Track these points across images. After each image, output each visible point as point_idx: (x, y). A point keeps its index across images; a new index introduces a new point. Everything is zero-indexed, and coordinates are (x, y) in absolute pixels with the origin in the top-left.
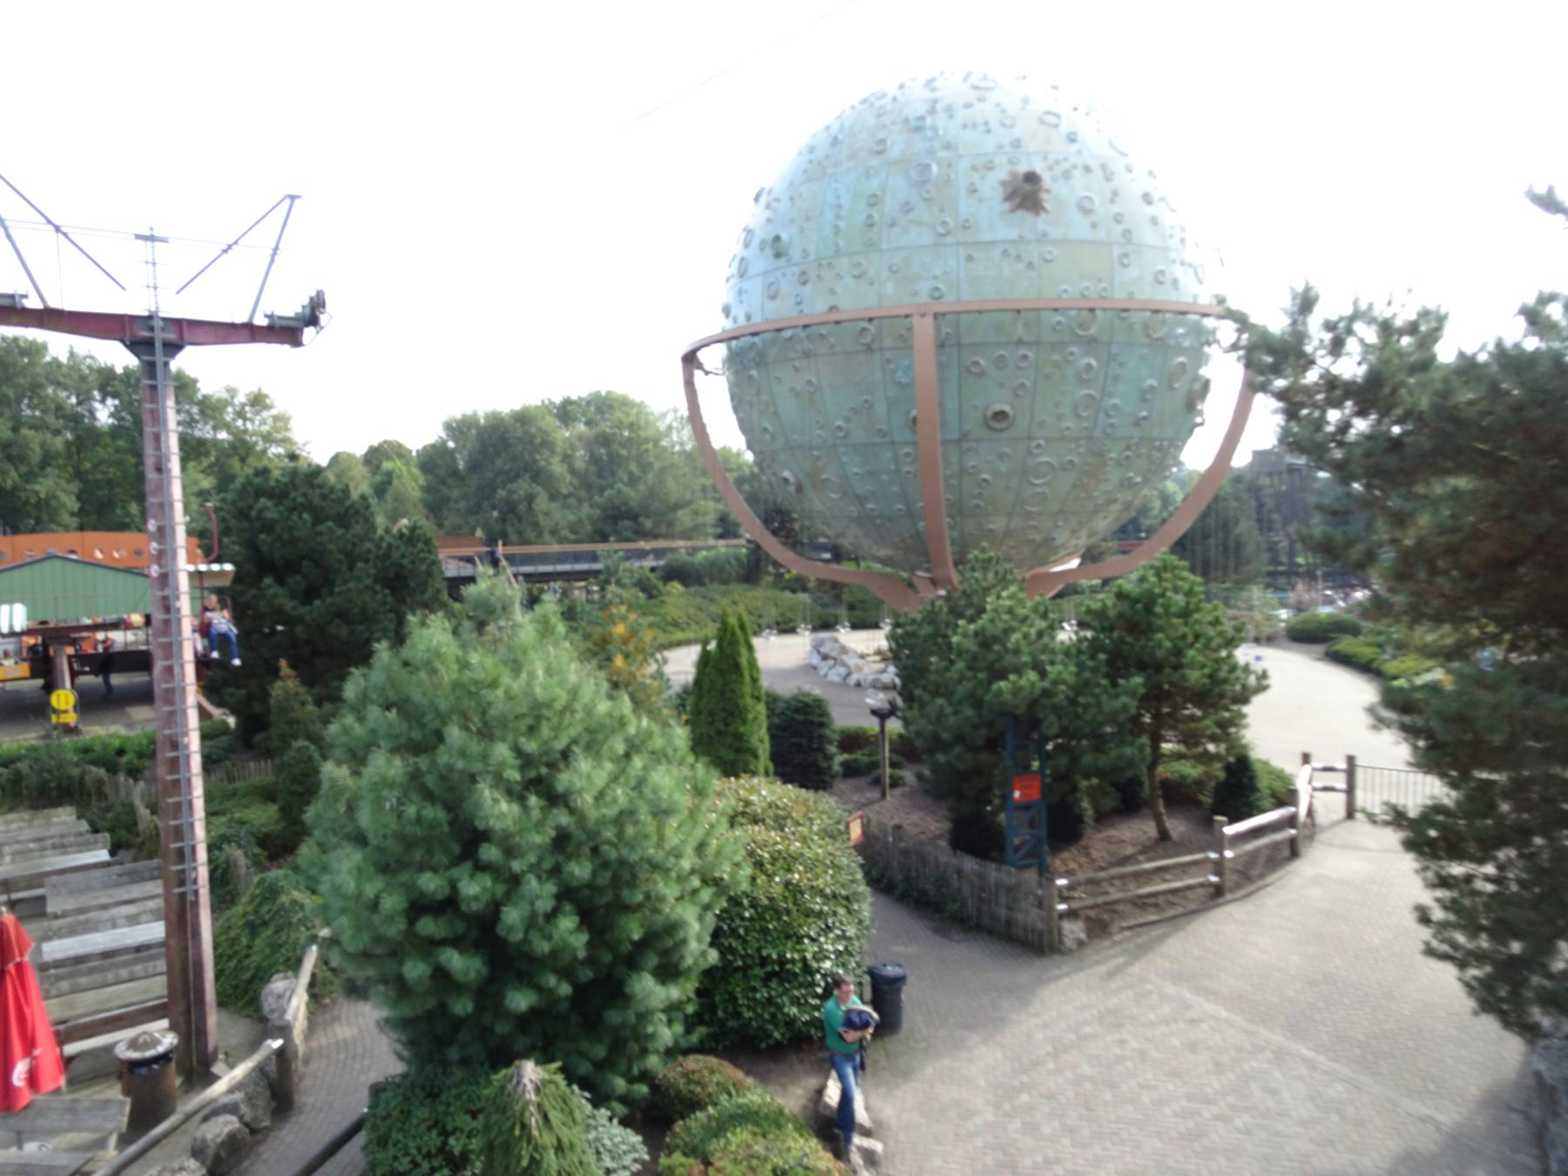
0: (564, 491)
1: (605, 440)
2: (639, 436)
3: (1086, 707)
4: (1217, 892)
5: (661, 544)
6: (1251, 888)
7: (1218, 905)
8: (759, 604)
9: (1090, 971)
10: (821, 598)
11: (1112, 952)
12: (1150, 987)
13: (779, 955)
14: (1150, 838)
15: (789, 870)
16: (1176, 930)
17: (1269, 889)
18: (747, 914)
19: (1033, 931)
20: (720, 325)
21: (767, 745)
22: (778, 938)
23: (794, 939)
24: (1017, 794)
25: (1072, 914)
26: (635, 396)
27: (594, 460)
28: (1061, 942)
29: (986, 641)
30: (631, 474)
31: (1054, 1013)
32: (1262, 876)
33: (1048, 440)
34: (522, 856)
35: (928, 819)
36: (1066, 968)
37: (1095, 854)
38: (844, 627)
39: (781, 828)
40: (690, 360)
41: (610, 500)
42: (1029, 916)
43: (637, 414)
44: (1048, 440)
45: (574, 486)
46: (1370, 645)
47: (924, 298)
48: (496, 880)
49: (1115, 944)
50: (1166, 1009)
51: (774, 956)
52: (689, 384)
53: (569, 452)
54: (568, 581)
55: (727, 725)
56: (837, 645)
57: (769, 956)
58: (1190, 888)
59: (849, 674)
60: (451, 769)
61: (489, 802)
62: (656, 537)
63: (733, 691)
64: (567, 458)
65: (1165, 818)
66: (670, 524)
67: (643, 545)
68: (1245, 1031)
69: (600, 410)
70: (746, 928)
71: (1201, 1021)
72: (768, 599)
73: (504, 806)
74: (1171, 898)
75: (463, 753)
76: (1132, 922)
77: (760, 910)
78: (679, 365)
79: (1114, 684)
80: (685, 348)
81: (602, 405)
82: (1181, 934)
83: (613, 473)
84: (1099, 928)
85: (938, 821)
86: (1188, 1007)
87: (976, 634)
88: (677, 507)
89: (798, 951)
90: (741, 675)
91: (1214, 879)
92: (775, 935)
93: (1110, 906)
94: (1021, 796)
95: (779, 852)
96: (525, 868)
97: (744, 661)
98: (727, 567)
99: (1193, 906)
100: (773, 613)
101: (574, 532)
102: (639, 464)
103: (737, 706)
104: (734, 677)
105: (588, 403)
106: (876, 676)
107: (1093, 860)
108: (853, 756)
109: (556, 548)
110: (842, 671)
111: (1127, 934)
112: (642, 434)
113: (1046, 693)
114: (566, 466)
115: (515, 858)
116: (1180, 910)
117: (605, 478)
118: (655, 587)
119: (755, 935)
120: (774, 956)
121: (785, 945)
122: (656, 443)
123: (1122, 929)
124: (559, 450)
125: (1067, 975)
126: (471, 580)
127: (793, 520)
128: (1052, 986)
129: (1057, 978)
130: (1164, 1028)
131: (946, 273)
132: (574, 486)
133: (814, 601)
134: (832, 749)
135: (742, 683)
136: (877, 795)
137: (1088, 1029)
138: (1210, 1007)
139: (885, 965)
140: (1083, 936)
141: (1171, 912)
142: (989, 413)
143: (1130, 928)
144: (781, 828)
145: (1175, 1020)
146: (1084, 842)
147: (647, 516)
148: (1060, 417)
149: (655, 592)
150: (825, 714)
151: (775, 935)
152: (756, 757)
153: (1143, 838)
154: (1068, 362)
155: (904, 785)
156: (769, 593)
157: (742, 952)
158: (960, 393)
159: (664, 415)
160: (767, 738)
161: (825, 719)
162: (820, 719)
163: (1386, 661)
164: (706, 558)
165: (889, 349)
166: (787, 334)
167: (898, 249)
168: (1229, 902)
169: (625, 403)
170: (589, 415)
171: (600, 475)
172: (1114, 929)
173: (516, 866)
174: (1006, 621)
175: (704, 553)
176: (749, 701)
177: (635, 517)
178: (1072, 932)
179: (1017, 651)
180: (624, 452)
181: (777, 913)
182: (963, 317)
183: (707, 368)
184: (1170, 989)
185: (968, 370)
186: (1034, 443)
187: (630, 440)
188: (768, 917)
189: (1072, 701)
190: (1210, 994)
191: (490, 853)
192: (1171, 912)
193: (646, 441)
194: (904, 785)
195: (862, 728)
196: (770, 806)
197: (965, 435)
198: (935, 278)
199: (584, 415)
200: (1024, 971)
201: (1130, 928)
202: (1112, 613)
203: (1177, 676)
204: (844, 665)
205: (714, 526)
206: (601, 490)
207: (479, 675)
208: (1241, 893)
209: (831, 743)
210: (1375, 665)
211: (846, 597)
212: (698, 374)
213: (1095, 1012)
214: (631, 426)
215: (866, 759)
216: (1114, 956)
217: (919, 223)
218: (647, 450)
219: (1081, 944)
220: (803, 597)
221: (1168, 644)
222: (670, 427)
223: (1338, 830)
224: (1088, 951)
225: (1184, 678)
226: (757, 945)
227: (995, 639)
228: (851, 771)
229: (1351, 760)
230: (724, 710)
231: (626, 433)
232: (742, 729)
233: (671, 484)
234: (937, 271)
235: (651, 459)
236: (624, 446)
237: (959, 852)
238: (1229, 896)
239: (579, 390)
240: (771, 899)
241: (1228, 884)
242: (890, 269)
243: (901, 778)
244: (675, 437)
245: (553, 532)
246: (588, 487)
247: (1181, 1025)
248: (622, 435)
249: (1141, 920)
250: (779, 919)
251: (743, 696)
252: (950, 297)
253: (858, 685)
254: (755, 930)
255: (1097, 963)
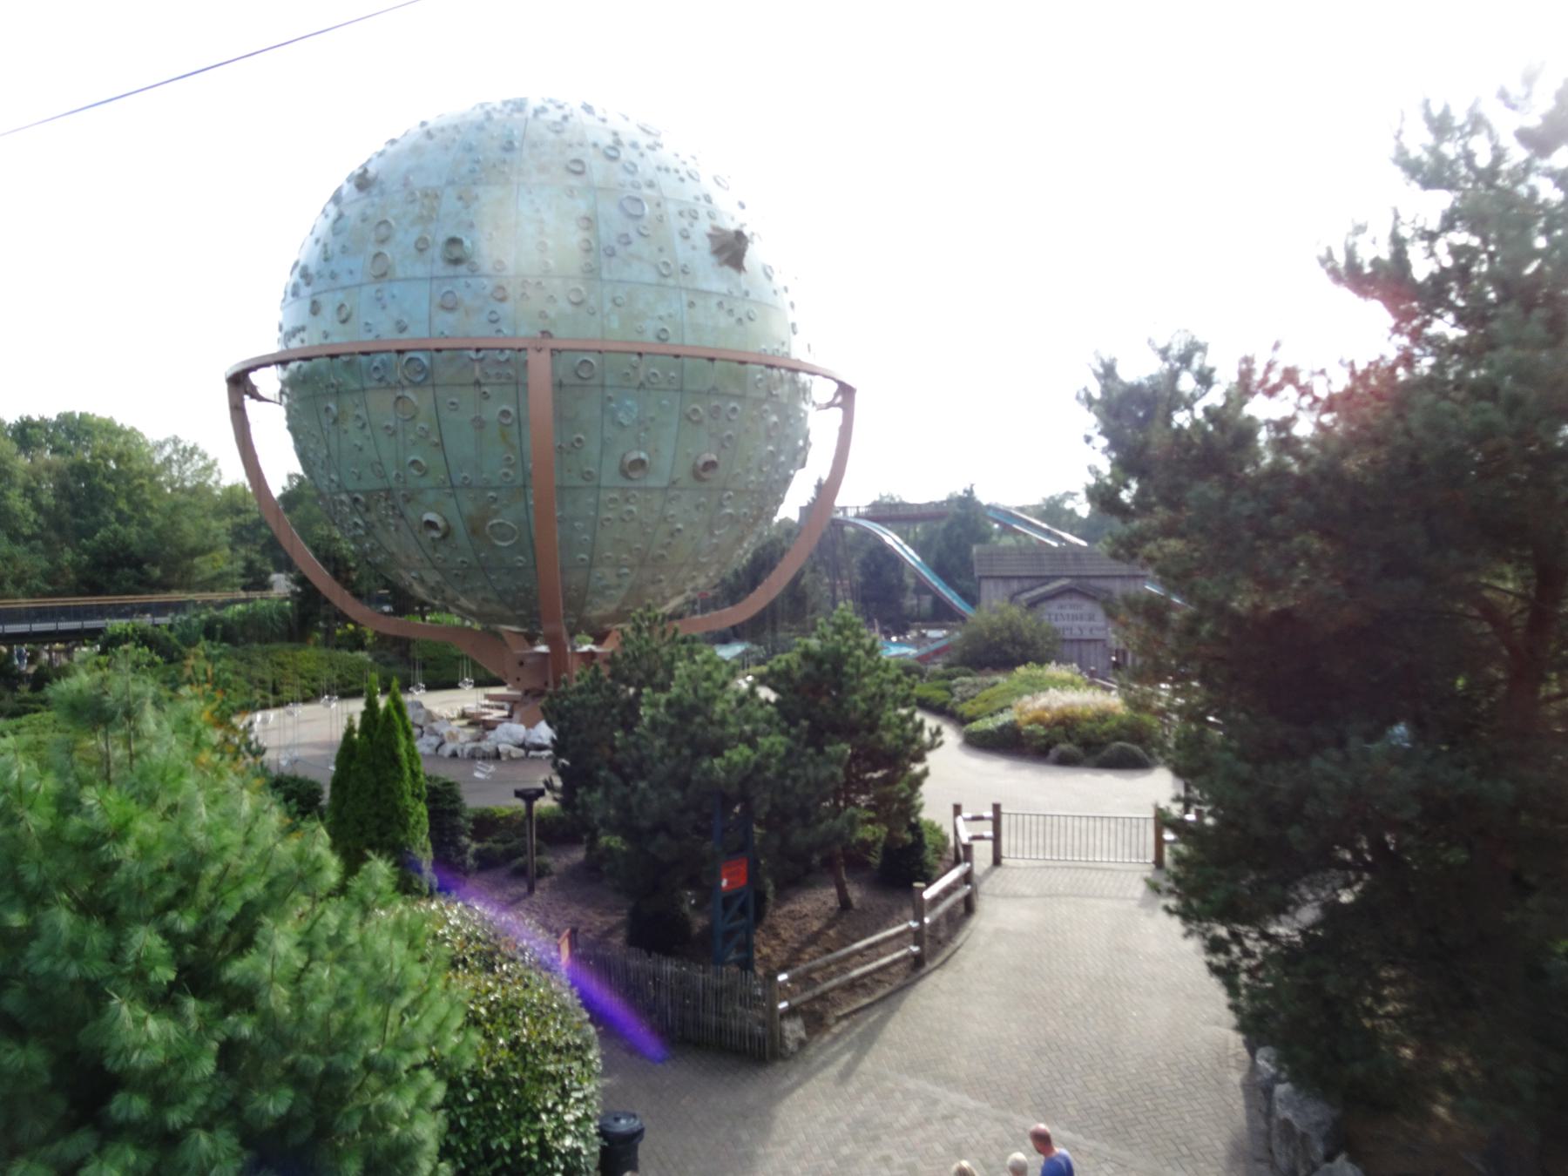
0: (26, 531)
1: (82, 471)
2: (130, 469)
3: (795, 779)
4: (917, 965)
5: (176, 596)
6: (947, 952)
7: (922, 977)
8: (311, 665)
9: (820, 1076)
10: (384, 656)
11: (836, 1048)
12: (890, 1085)
13: (511, 1142)
14: (831, 909)
15: (513, 1025)
16: (892, 1012)
17: (961, 952)
18: (470, 1098)
19: (751, 1037)
20: (272, 345)
21: (430, 854)
22: (509, 1120)
23: (528, 1116)
24: (724, 883)
25: (791, 1012)
26: (123, 420)
27: (63, 491)
28: (783, 1045)
29: (683, 712)
30: (120, 513)
31: (802, 1137)
32: (950, 938)
33: (735, 491)
34: (183, 1100)
35: (590, 912)
36: (795, 1077)
37: (785, 935)
38: (418, 690)
39: (489, 968)
40: (239, 383)
41: (103, 543)
42: (749, 1020)
43: (125, 443)
44: (735, 491)
45: (40, 526)
46: (939, 688)
47: (650, 337)
48: (141, 1147)
49: (836, 1038)
50: (914, 1109)
51: (507, 1147)
52: (238, 412)
53: (34, 484)
54: (36, 643)
55: (382, 834)
56: (421, 711)
57: (500, 1146)
58: (895, 962)
59: (442, 743)
60: (53, 978)
61: (129, 1024)
62: (167, 588)
63: (390, 791)
64: (30, 492)
65: (847, 886)
66: (189, 571)
67: (145, 598)
68: (997, 1119)
69: (71, 434)
70: (468, 1116)
71: (953, 1117)
72: (322, 658)
73: (152, 1026)
74: (876, 976)
75: (76, 951)
76: (846, 1010)
77: (484, 1088)
78: (223, 388)
79: (820, 751)
80: (232, 364)
81: (75, 429)
82: (898, 1016)
83: (95, 512)
84: (816, 1021)
85: (601, 914)
86: (935, 1102)
87: (669, 704)
88: (195, 552)
89: (533, 1132)
90: (400, 770)
91: (915, 949)
92: (505, 1117)
93: (823, 997)
94: (729, 884)
95: (496, 1001)
96: (189, 1119)
97: (402, 751)
98: (269, 623)
99: (898, 982)
100: (328, 675)
101: (53, 582)
102: (129, 501)
103: (395, 808)
104: (392, 773)
105: (57, 425)
106: (473, 745)
107: (784, 941)
108: (486, 845)
109: (24, 603)
110: (434, 740)
111: (845, 1023)
112: (135, 466)
113: (759, 768)
114: (29, 501)
115: (171, 1104)
116: (888, 988)
117: (83, 517)
118: (176, 648)
119: (480, 1122)
120: (507, 1147)
121: (518, 1128)
122: (152, 477)
123: (839, 1019)
124: (19, 481)
125: (799, 1084)
126: (63, 673)
127: (349, 570)
128: (787, 1102)
129: (791, 1090)
130: (920, 1134)
131: (670, 316)
132: (40, 526)
133: (376, 660)
134: (465, 840)
135: (402, 780)
136: (523, 889)
137: (845, 1151)
138: (957, 1098)
139: (617, 1119)
140: (803, 1034)
141: (880, 993)
142: (701, 463)
143: (846, 1016)
144: (489, 968)
145: (928, 1120)
146: (767, 921)
147: (155, 564)
148: (748, 471)
149: (176, 654)
150: (457, 799)
151: (505, 1117)
152: (419, 871)
153: (824, 909)
154: (763, 418)
155: (551, 874)
156: (323, 652)
157: (464, 1150)
158: (520, 434)
159: (161, 446)
160: (429, 846)
161: (457, 806)
162: (452, 806)
163: (956, 704)
164: (240, 613)
165: (612, 387)
166: (378, 360)
167: (620, 281)
168: (930, 972)
169: (109, 429)
170: (58, 442)
171: (75, 513)
172: (831, 1021)
173: (175, 1118)
174: (707, 689)
175: (239, 607)
176: (409, 800)
177: (137, 564)
178: (793, 1032)
179: (723, 722)
180: (111, 487)
181: (504, 1084)
182: (687, 361)
183: (261, 392)
184: (911, 1084)
185: (689, 418)
186: (726, 495)
187: (118, 473)
188: (494, 1095)
189: (782, 775)
190: (950, 1081)
191: (133, 1106)
192: (880, 993)
193: (141, 474)
194: (551, 874)
195: (487, 810)
196: (468, 939)
197: (674, 483)
198: (661, 318)
199: (49, 441)
200: (752, 1090)
201: (846, 1016)
202: (797, 675)
203: (872, 738)
204: (434, 733)
205: (243, 576)
206: (90, 532)
207: (98, 821)
208: (939, 960)
209: (463, 833)
210: (948, 707)
211: (417, 655)
212: (250, 404)
213: (843, 1126)
214: (119, 458)
215: (500, 847)
216: (840, 1053)
217: (640, 258)
218: (141, 485)
219: (802, 1044)
220: (363, 655)
221: (863, 706)
222: (169, 460)
223: (992, 877)
224: (812, 1050)
225: (880, 739)
226: (483, 1136)
227: (695, 710)
228: (486, 862)
229: (996, 808)
230: (377, 815)
231: (112, 464)
232: (402, 838)
233: (187, 526)
234: (662, 312)
235: (147, 496)
236: (109, 481)
237: (654, 955)
238: (929, 965)
239: (46, 408)
240: (499, 1070)
241: (927, 951)
242: (614, 301)
243: (546, 866)
244: (175, 471)
245: (18, 582)
246: (59, 526)
247: (937, 1126)
248: (107, 466)
249: (855, 1006)
250: (507, 1093)
251: (402, 796)
252: (673, 340)
253: (454, 755)
254: (480, 1116)
255: (825, 1064)
